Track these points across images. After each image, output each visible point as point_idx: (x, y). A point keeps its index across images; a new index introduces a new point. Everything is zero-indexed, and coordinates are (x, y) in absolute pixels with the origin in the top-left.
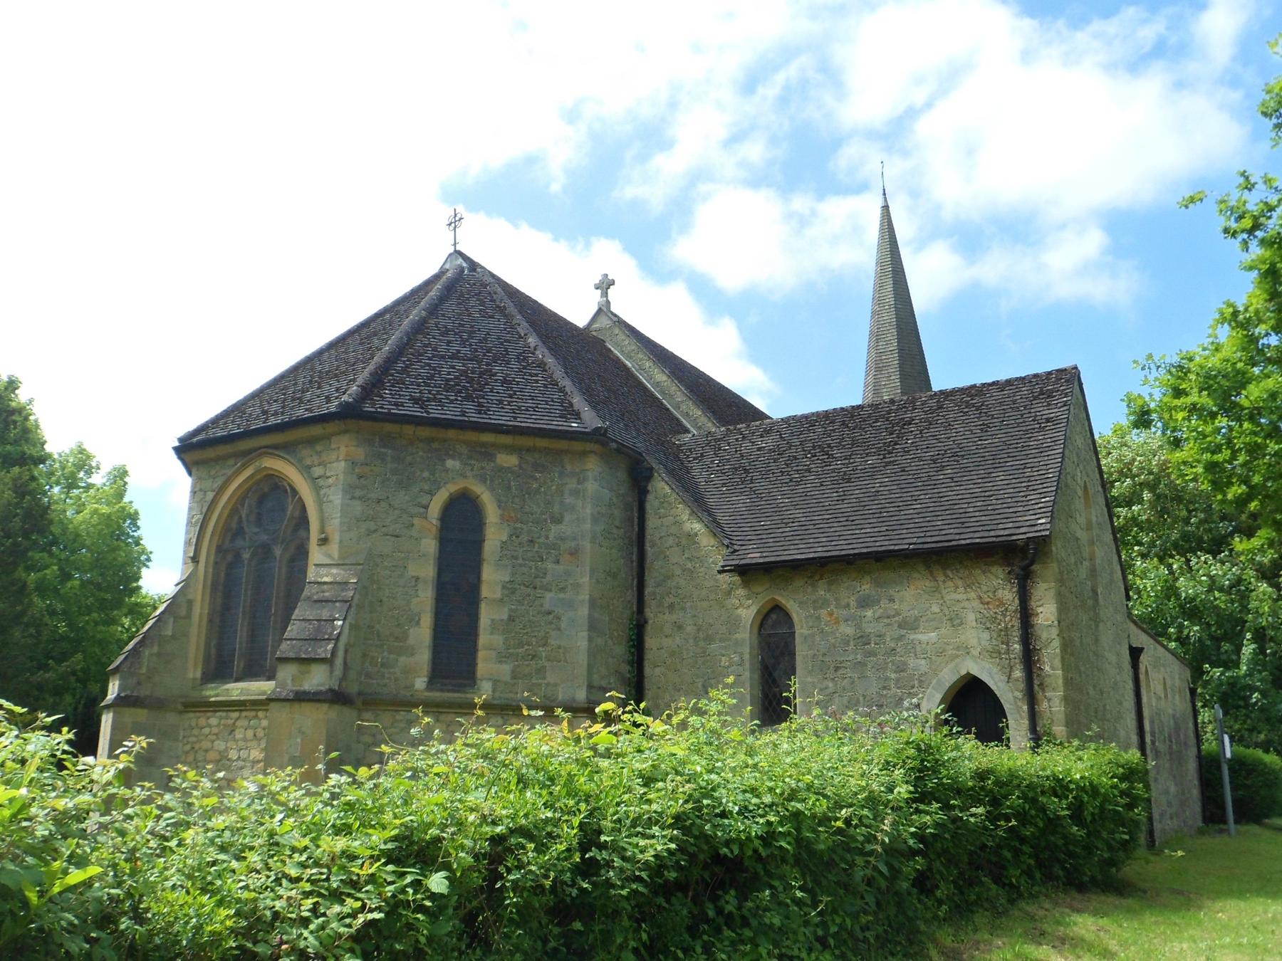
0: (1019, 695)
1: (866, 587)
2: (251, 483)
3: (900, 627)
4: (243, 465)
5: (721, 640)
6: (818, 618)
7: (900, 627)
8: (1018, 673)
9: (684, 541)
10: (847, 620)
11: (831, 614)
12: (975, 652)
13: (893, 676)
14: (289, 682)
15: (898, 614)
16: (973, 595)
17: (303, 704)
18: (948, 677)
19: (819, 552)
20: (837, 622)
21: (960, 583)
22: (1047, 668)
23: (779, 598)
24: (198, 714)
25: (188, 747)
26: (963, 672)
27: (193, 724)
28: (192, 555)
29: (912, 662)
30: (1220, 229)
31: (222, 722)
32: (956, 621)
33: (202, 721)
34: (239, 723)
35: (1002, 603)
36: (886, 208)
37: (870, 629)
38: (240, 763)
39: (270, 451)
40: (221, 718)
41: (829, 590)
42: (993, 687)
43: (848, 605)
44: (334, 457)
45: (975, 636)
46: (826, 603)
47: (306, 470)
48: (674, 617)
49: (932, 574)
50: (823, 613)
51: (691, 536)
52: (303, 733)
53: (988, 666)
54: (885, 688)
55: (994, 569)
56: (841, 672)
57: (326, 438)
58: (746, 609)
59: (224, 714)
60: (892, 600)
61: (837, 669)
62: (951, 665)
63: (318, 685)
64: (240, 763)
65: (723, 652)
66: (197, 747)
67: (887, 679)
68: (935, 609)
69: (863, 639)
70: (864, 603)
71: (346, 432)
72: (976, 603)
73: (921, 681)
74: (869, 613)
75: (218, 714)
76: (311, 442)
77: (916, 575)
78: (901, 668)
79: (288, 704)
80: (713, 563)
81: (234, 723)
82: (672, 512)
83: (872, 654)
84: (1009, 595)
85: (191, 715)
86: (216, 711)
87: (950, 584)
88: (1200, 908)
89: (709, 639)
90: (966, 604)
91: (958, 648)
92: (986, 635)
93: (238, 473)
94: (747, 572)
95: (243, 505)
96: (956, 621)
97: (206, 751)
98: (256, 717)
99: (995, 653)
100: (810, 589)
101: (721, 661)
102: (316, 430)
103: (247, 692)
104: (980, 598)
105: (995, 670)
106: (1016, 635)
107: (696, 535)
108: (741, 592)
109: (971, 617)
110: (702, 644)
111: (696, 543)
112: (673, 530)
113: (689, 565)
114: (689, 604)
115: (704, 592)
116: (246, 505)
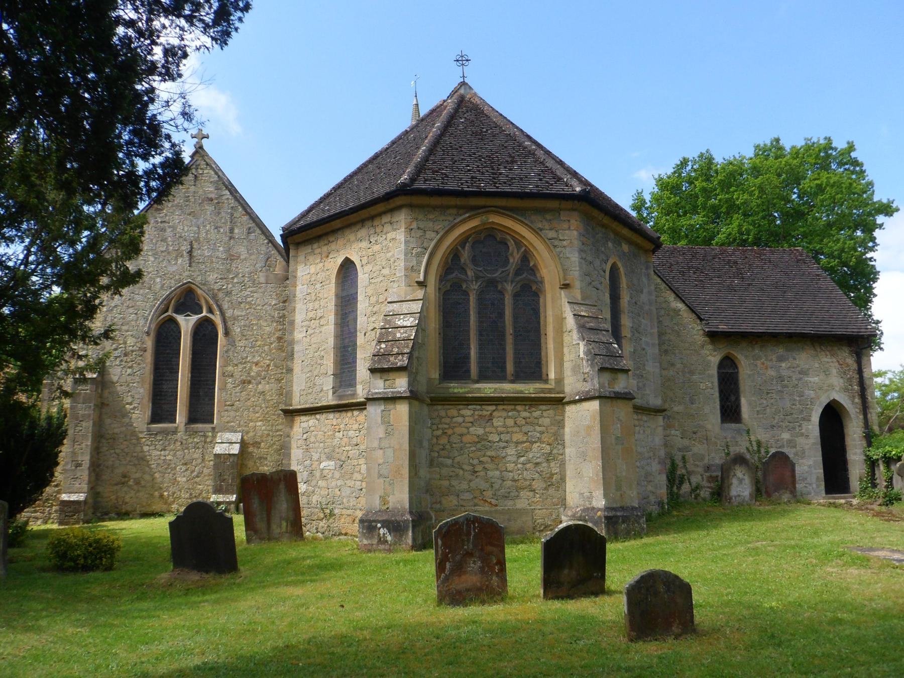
0: (858, 411)
1: (781, 351)
2: (473, 231)
3: (799, 373)
4: (469, 217)
5: (699, 374)
6: (756, 365)
7: (799, 373)
8: (857, 400)
9: (672, 313)
10: (772, 368)
11: (763, 364)
12: (837, 389)
13: (798, 398)
14: (606, 385)
15: (798, 366)
16: (834, 360)
17: (618, 401)
18: (824, 401)
19: (761, 329)
20: (766, 368)
21: (828, 353)
22: (869, 398)
23: (732, 352)
24: (445, 407)
25: (439, 432)
26: (832, 398)
27: (443, 413)
28: (421, 278)
29: (807, 392)
30: (687, 156)
31: (476, 413)
32: (827, 373)
33: (453, 412)
34: (495, 414)
35: (848, 366)
36: (417, 105)
37: (785, 373)
38: (502, 444)
39: (499, 210)
40: (474, 410)
41: (761, 351)
42: (846, 406)
43: (771, 360)
44: (566, 226)
45: (836, 381)
46: (759, 358)
47: (537, 232)
48: (669, 358)
49: (814, 347)
50: (759, 363)
51: (677, 312)
52: (621, 421)
53: (843, 395)
54: (793, 404)
55: (843, 348)
56: (769, 395)
57: (558, 211)
58: (714, 359)
59: (479, 407)
60: (795, 359)
61: (768, 393)
62: (826, 395)
63: (624, 388)
64: (502, 444)
65: (701, 381)
66: (450, 432)
67: (795, 400)
68: (817, 365)
69: (781, 378)
70: (781, 359)
71: (574, 210)
72: (836, 364)
73: (811, 402)
74: (783, 365)
75: (470, 407)
76: (542, 211)
77: (806, 347)
78: (801, 395)
79: (609, 400)
80: (692, 328)
81: (491, 414)
82: (663, 295)
83: (786, 386)
84: (851, 361)
85: (439, 407)
86: (468, 405)
87: (823, 353)
88: (722, 527)
89: (692, 373)
90: (831, 364)
91: (829, 386)
92: (841, 381)
93: (463, 221)
94: (714, 336)
95: (463, 248)
96: (827, 373)
97: (461, 435)
98: (515, 410)
99: (846, 390)
100: (750, 349)
101: (700, 386)
102: (554, 204)
103: (502, 391)
104: (838, 362)
105: (846, 398)
106: (855, 381)
107: (680, 310)
108: (710, 347)
109: (834, 371)
110: (687, 375)
111: (679, 315)
112: (664, 305)
113: (676, 328)
114: (677, 351)
115: (687, 345)
116: (466, 248)
